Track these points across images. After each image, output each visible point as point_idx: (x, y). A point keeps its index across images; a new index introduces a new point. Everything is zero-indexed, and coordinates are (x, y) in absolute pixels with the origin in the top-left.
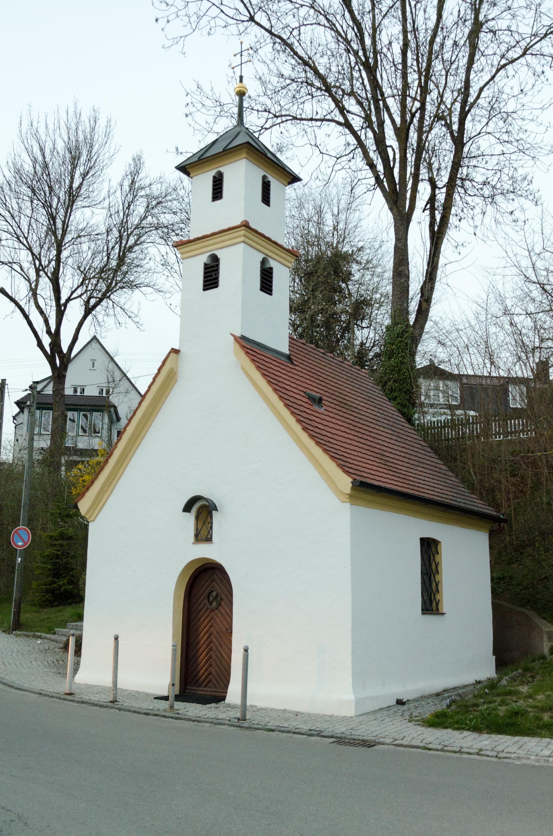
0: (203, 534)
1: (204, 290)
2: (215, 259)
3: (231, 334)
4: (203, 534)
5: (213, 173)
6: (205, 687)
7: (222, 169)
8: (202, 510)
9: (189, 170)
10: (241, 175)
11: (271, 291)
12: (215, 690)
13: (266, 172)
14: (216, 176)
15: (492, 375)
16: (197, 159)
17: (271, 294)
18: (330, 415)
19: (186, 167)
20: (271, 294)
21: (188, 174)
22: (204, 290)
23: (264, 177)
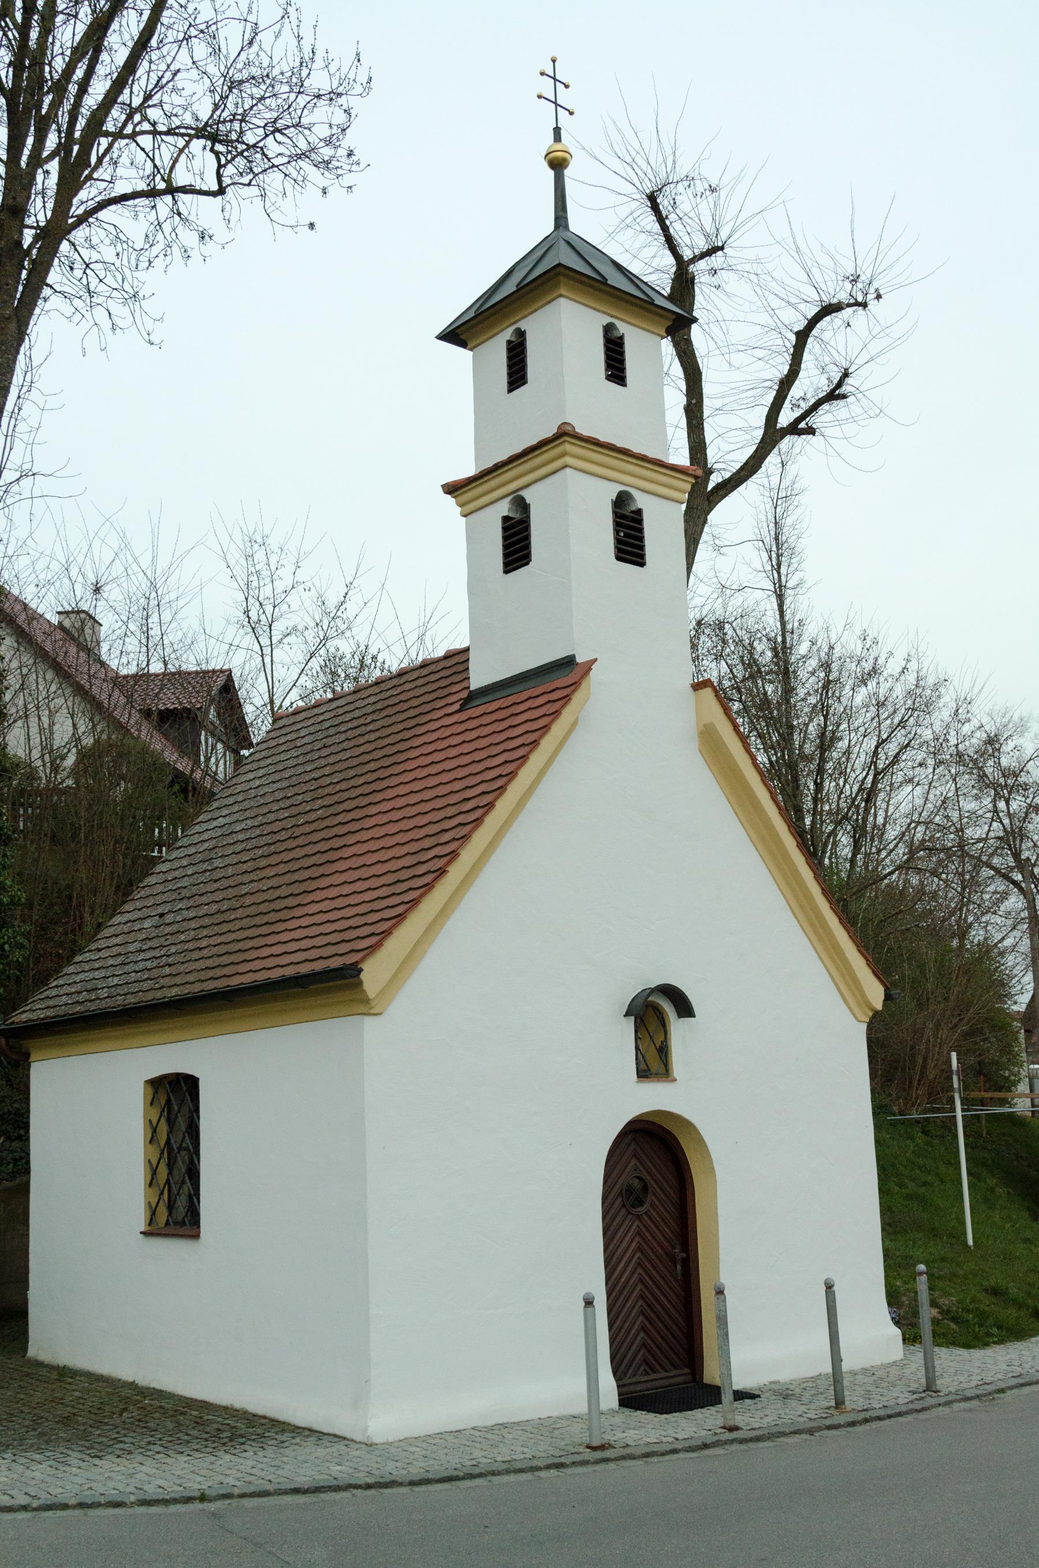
0: (654, 1062)
1: (506, 572)
2: (522, 505)
3: (596, 660)
4: (654, 1062)
5: (507, 334)
6: (634, 1375)
7: (523, 325)
8: (655, 1015)
9: (463, 337)
10: (566, 333)
11: (642, 556)
12: (665, 1374)
13: (612, 316)
14: (513, 339)
15: (170, 197)
16: (473, 315)
17: (642, 564)
18: (454, 743)
19: (458, 331)
20: (642, 564)
21: (463, 344)
22: (506, 572)
23: (608, 329)
